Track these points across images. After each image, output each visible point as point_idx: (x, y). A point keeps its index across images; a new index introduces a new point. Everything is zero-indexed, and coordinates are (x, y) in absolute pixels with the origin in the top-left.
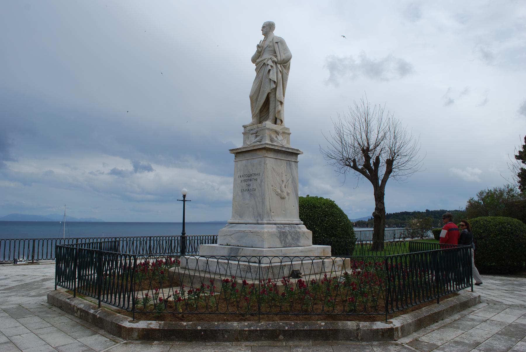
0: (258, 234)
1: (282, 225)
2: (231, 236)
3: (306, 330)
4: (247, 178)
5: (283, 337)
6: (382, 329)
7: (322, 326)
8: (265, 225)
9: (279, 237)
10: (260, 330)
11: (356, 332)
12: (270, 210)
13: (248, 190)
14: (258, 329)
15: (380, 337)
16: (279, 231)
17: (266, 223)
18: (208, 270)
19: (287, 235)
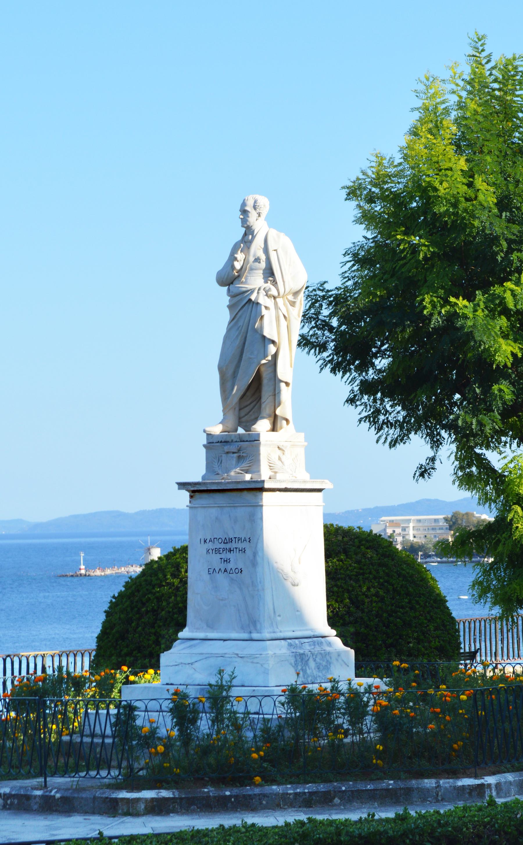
0: (255, 661)
1: (297, 641)
2: (193, 666)
3: (368, 790)
4: (222, 546)
5: (339, 801)
6: (469, 785)
7: (390, 784)
8: (268, 642)
9: (294, 665)
10: (308, 792)
11: (435, 791)
12: (274, 612)
13: (225, 571)
14: (306, 791)
15: (467, 795)
16: (293, 653)
17: (270, 638)
18: (261, 712)
19: (308, 660)
